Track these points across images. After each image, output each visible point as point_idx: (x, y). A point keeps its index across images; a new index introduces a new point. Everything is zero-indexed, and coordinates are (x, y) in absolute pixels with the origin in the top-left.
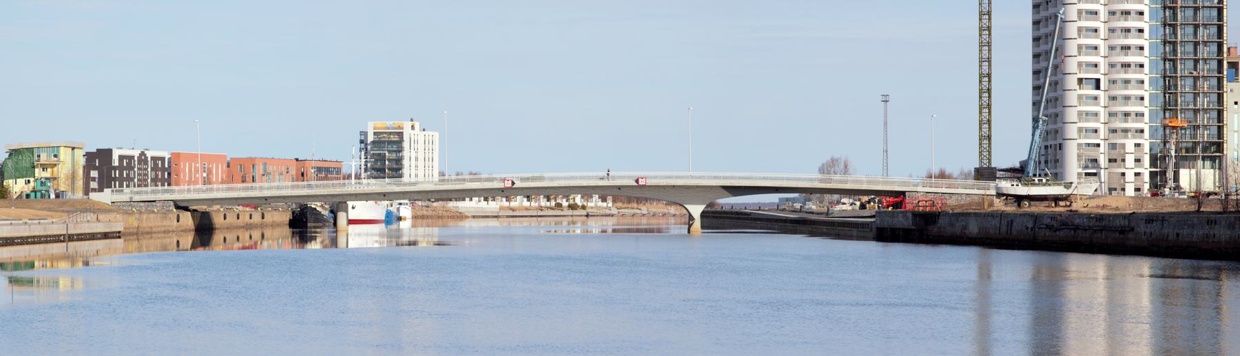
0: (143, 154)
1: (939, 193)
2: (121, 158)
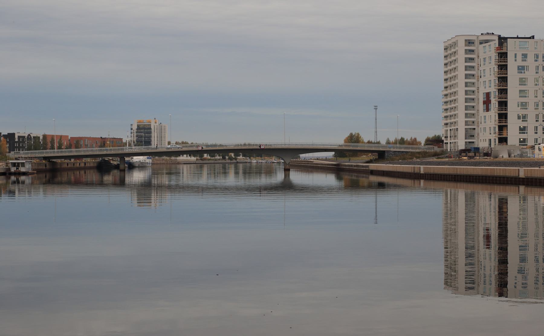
0: (29, 135)
2: (19, 137)
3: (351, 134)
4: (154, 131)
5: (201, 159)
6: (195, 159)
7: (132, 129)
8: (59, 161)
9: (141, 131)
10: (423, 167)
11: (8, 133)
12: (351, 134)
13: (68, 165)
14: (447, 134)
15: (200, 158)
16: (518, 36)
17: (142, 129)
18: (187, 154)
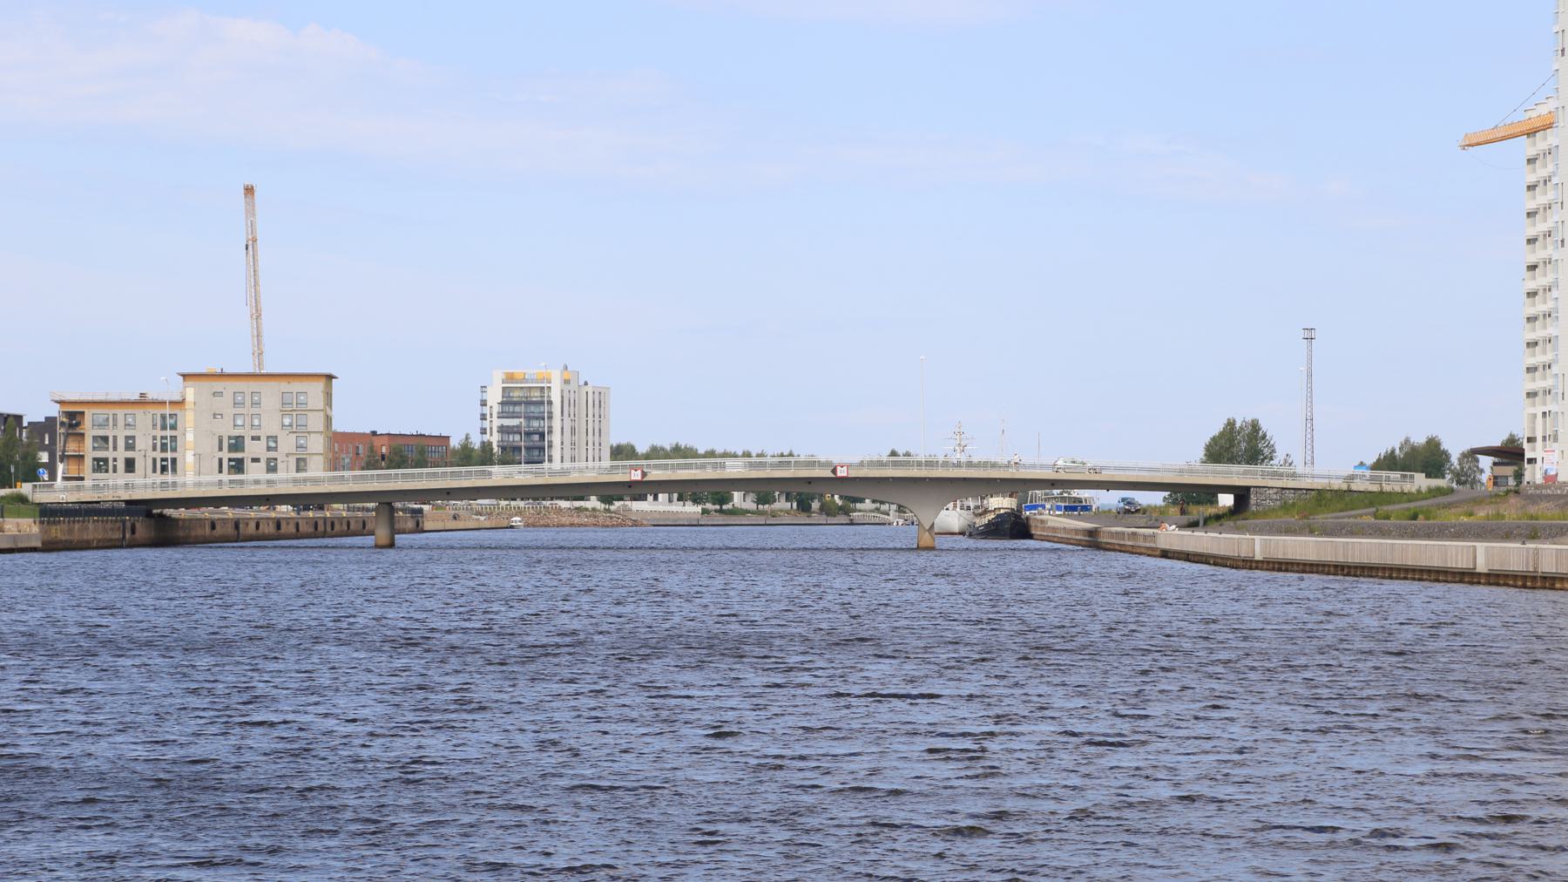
1: (1302, 489)
3: (1231, 424)
4: (562, 412)
5: (721, 511)
6: (699, 509)
7: (484, 403)
8: (181, 513)
9: (517, 409)
10: (1486, 547)
11: (46, 418)
12: (1231, 424)
13: (213, 527)
14: (1533, 429)
15: (718, 507)
16: (142, 395)
17: (519, 403)
18: (670, 493)
